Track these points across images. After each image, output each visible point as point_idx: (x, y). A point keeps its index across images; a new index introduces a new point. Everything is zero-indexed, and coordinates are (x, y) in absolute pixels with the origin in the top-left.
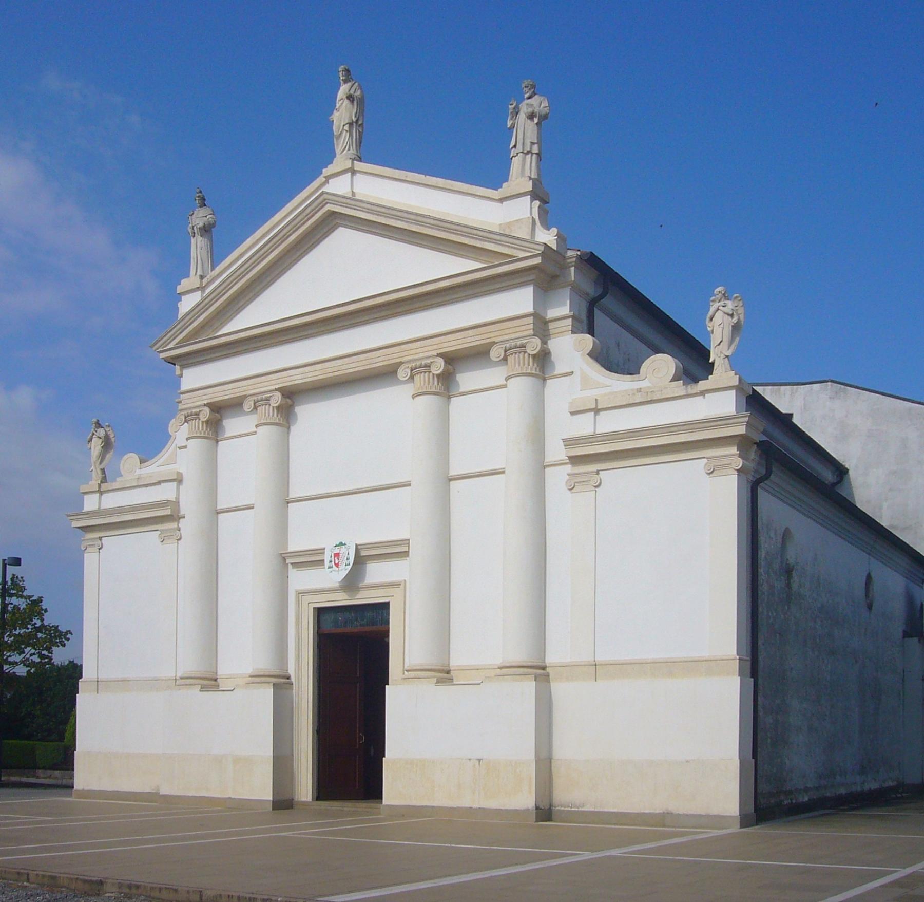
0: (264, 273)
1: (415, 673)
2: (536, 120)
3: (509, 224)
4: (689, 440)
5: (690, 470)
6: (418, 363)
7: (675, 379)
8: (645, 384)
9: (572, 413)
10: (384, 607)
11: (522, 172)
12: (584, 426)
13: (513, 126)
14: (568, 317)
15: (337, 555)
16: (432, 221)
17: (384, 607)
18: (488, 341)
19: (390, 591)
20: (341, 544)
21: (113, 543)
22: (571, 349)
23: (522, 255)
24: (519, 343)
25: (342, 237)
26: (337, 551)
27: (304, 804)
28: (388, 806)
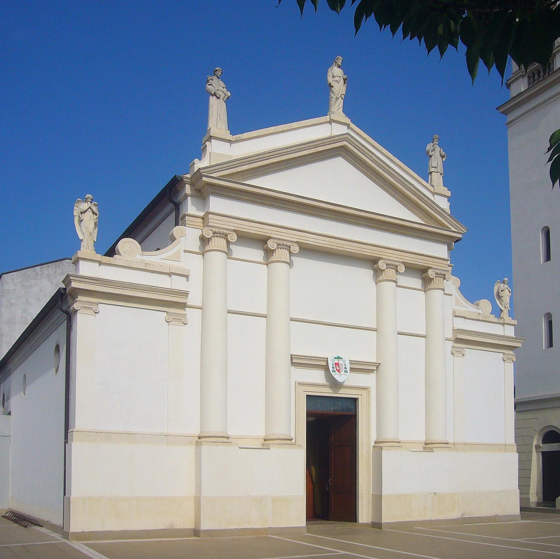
0: (395, 188)
4: (136, 295)
6: (221, 231)
10: (355, 401)
12: (461, 324)
15: (337, 364)
16: (413, 188)
17: (355, 401)
18: (378, 256)
19: (360, 392)
20: (338, 358)
21: (109, 311)
23: (454, 229)
25: (340, 163)
26: (336, 361)
28: (74, 533)
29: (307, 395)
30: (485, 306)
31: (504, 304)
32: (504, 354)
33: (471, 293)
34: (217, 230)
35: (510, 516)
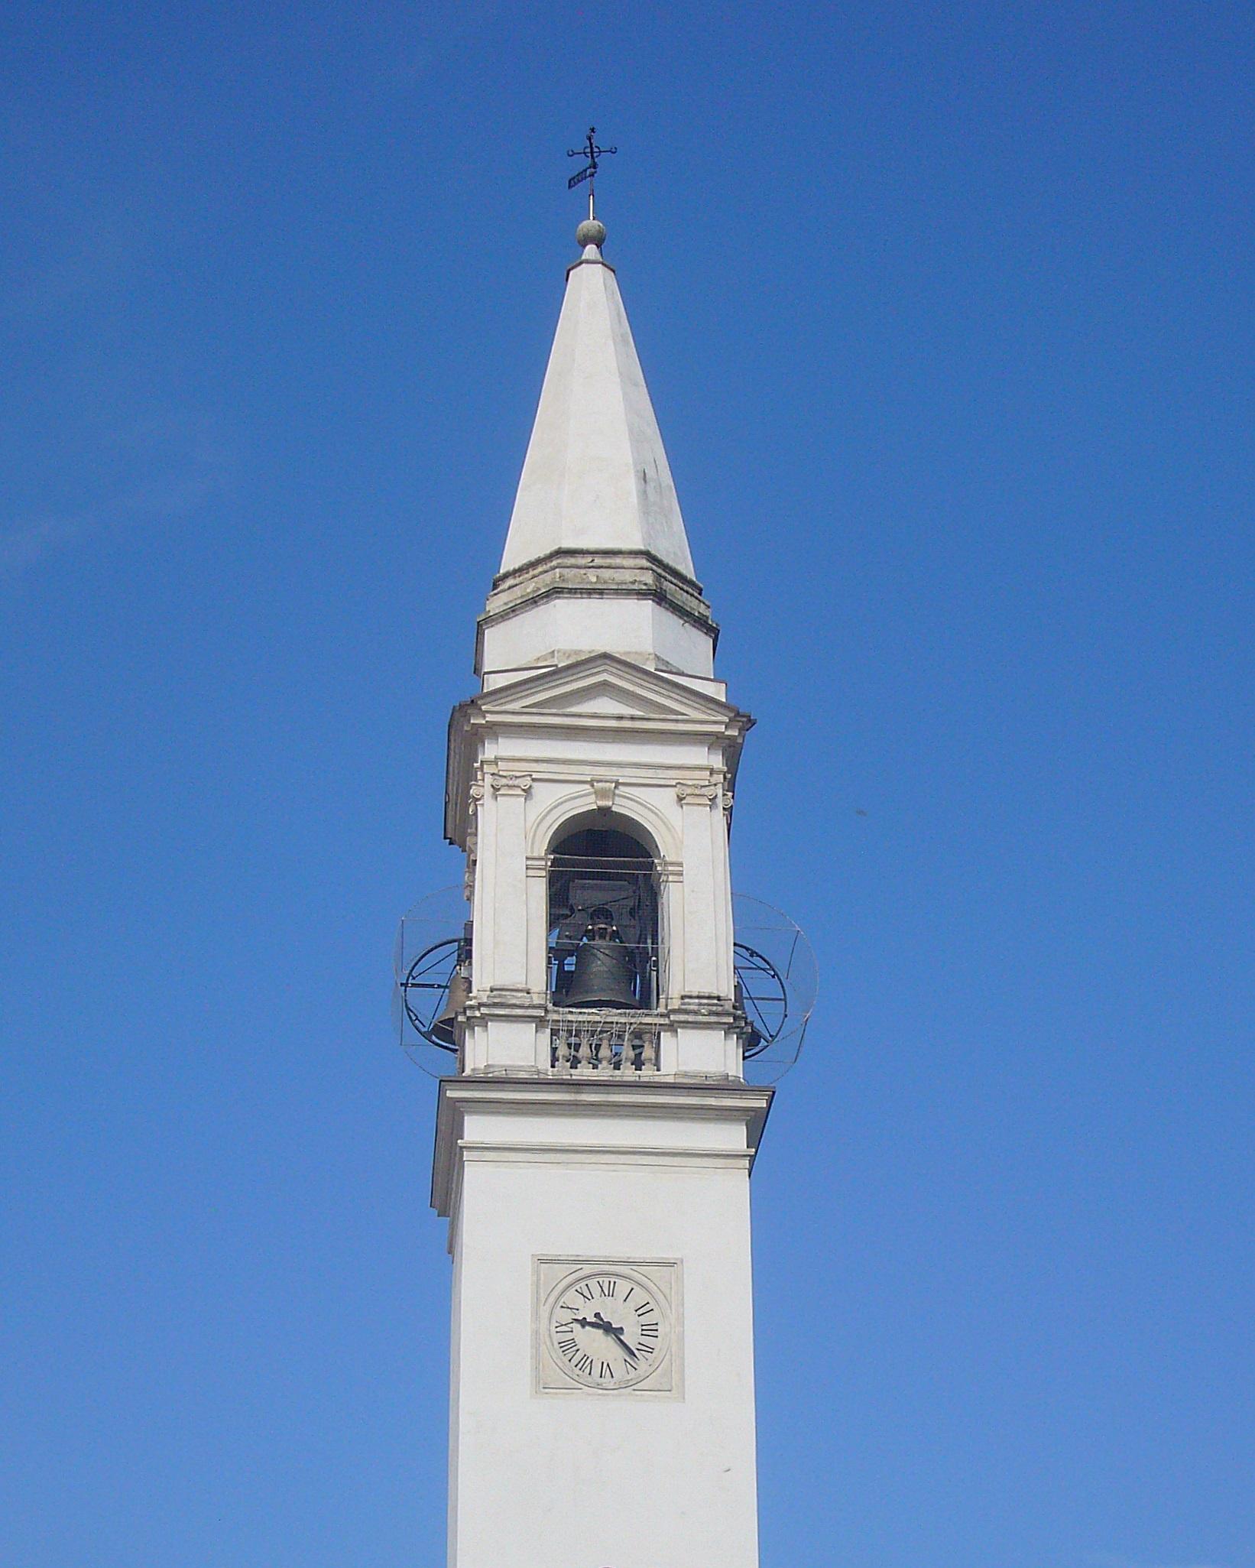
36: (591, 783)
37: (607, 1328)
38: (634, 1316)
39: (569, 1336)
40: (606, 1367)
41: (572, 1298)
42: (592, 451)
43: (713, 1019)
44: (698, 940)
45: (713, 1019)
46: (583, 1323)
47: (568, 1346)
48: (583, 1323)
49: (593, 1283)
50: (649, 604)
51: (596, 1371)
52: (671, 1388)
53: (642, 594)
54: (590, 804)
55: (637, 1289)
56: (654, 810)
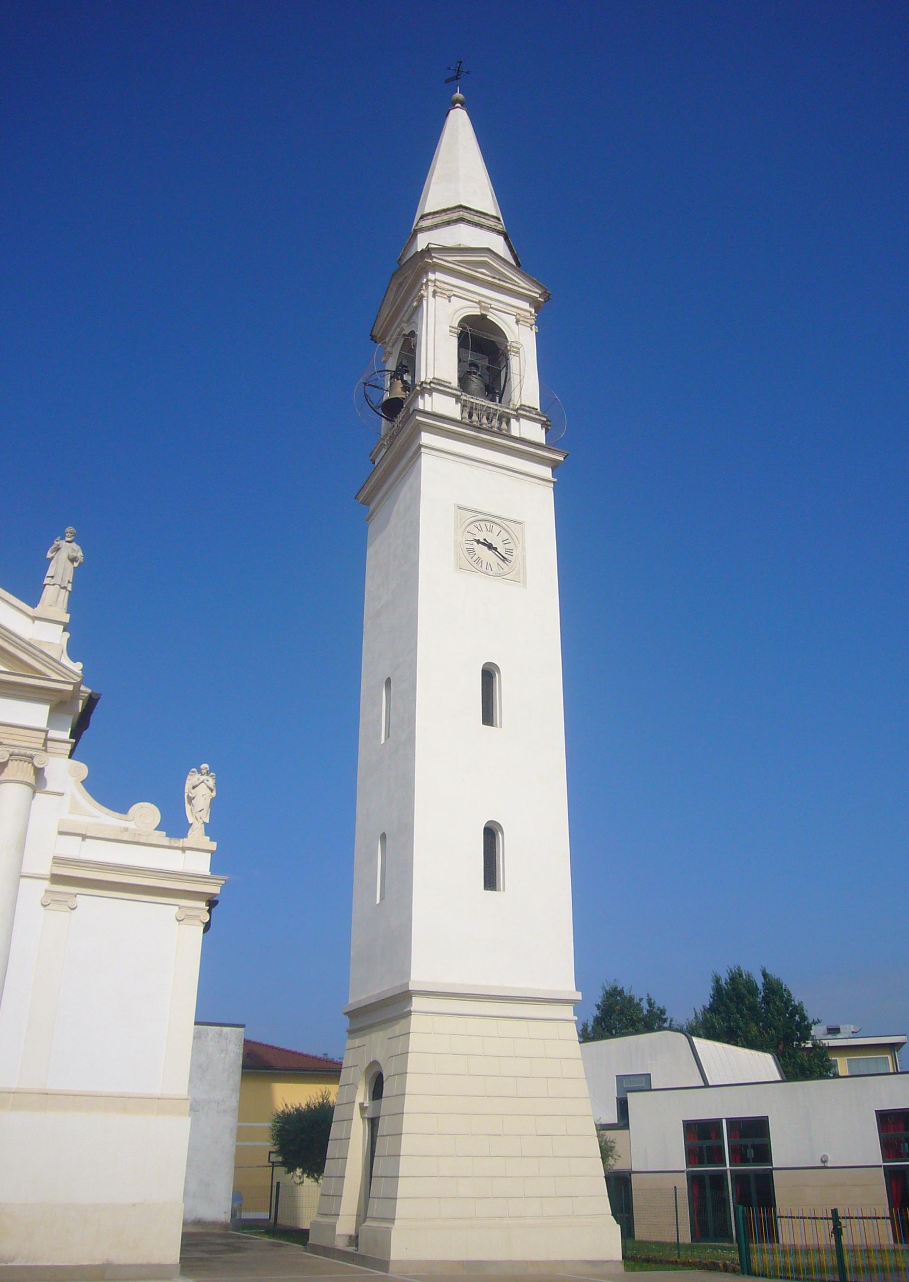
1: (222, 1031)
2: (76, 564)
3: (40, 642)
5: (168, 910)
6: (23, 751)
7: (158, 828)
8: (131, 825)
9: (61, 833)
11: (55, 599)
12: (73, 848)
13: (53, 558)
14: (68, 742)
22: (65, 772)
23: (54, 676)
24: (29, 752)
27: (270, 1097)
29: (885, 1118)
30: (146, 815)
31: (194, 812)
32: (180, 907)
33: (110, 790)
34: (16, 751)
35: (149, 1266)
36: (479, 303)
37: (490, 547)
38: (502, 544)
39: (471, 547)
40: (488, 565)
41: (472, 528)
42: (459, 171)
43: (537, 417)
44: (525, 381)
45: (537, 417)
46: (478, 542)
47: (471, 551)
48: (478, 542)
49: (482, 524)
50: (501, 239)
51: (484, 565)
52: (520, 580)
53: (499, 232)
54: (477, 312)
55: (503, 531)
56: (505, 322)
